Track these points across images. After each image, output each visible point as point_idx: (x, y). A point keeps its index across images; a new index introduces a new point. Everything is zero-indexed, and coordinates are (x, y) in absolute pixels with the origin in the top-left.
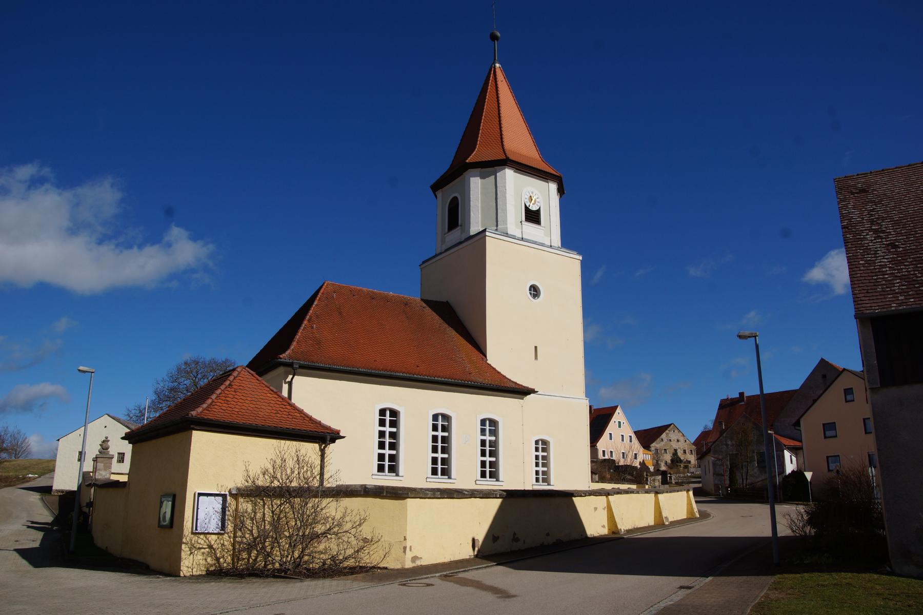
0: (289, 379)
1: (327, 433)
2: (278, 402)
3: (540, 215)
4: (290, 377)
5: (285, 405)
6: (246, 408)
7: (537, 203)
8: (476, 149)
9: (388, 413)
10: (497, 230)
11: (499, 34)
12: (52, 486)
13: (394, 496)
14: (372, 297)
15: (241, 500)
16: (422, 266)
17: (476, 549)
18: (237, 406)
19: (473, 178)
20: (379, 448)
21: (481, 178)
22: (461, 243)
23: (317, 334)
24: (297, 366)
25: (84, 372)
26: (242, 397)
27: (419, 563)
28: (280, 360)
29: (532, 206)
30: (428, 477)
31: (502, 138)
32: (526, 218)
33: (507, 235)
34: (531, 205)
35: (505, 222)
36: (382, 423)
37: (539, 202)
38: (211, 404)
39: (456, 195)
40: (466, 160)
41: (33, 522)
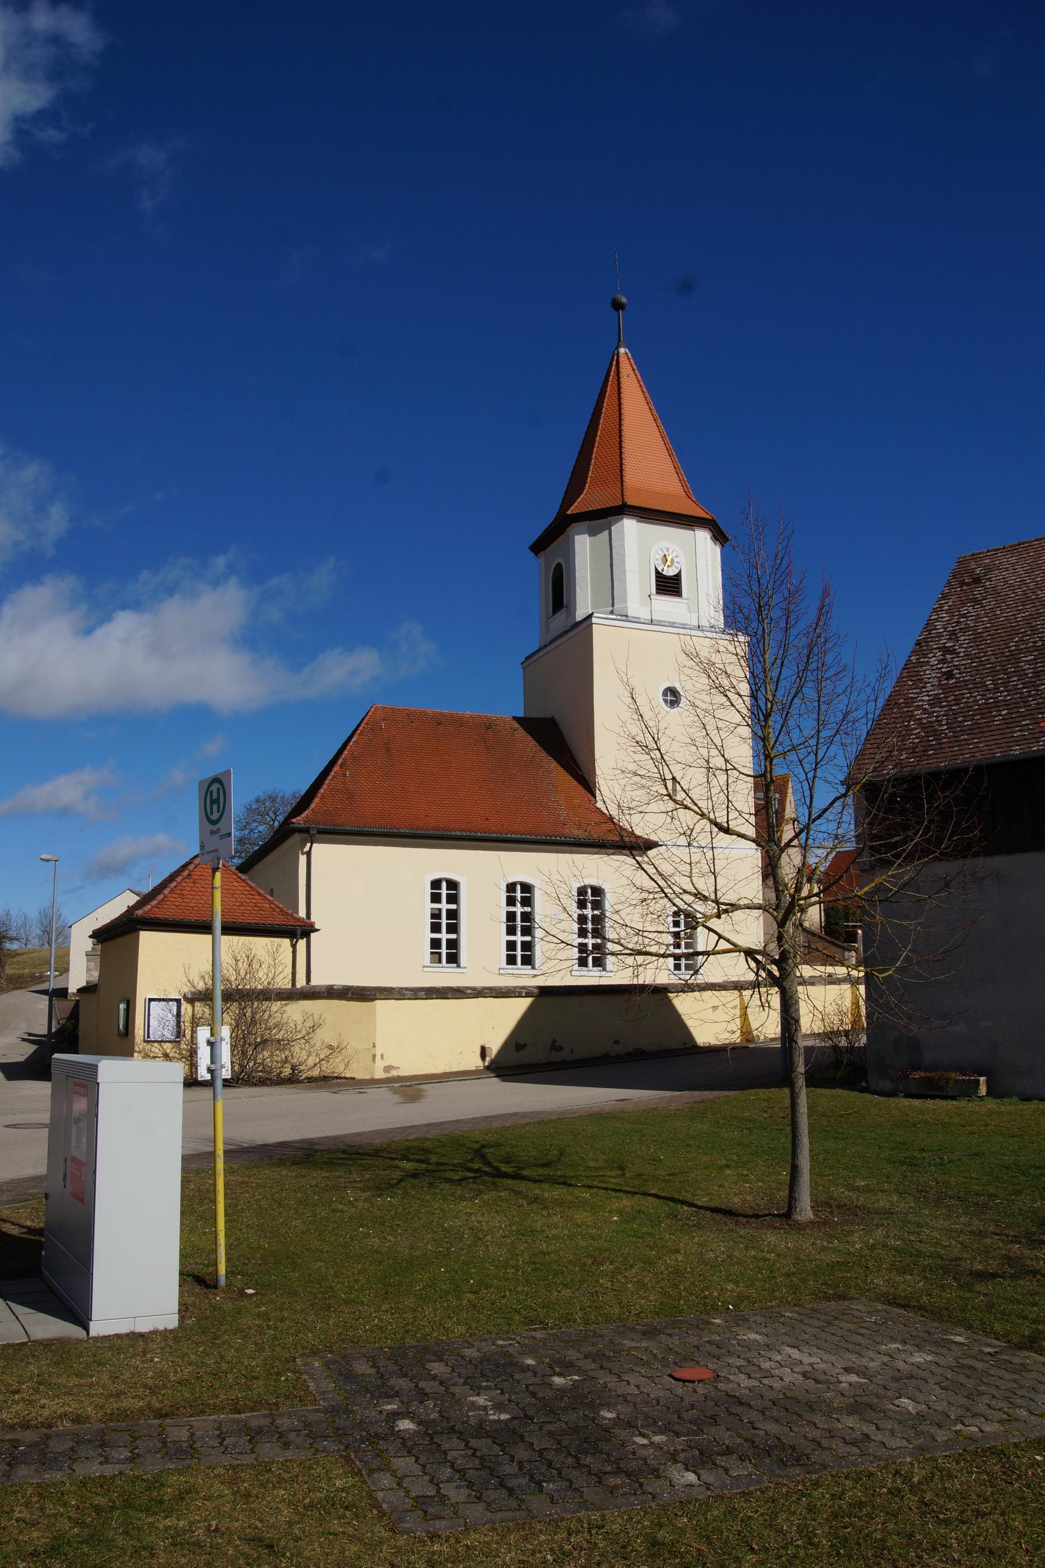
0: (307, 849)
2: (244, 892)
4: (309, 845)
6: (203, 902)
7: (675, 564)
8: (586, 491)
9: (444, 885)
10: (612, 613)
11: (624, 300)
12: (67, 989)
14: (440, 721)
15: (197, 1004)
17: (488, 1059)
18: (193, 901)
20: (508, 934)
22: (566, 632)
25: (48, 861)
26: (202, 889)
27: (394, 1073)
28: (292, 825)
29: (668, 571)
31: (621, 471)
32: (657, 589)
33: (625, 617)
34: (665, 568)
35: (624, 599)
36: (436, 898)
37: (678, 563)
38: (162, 900)
39: (560, 560)
40: (568, 510)
41: (30, 1035)
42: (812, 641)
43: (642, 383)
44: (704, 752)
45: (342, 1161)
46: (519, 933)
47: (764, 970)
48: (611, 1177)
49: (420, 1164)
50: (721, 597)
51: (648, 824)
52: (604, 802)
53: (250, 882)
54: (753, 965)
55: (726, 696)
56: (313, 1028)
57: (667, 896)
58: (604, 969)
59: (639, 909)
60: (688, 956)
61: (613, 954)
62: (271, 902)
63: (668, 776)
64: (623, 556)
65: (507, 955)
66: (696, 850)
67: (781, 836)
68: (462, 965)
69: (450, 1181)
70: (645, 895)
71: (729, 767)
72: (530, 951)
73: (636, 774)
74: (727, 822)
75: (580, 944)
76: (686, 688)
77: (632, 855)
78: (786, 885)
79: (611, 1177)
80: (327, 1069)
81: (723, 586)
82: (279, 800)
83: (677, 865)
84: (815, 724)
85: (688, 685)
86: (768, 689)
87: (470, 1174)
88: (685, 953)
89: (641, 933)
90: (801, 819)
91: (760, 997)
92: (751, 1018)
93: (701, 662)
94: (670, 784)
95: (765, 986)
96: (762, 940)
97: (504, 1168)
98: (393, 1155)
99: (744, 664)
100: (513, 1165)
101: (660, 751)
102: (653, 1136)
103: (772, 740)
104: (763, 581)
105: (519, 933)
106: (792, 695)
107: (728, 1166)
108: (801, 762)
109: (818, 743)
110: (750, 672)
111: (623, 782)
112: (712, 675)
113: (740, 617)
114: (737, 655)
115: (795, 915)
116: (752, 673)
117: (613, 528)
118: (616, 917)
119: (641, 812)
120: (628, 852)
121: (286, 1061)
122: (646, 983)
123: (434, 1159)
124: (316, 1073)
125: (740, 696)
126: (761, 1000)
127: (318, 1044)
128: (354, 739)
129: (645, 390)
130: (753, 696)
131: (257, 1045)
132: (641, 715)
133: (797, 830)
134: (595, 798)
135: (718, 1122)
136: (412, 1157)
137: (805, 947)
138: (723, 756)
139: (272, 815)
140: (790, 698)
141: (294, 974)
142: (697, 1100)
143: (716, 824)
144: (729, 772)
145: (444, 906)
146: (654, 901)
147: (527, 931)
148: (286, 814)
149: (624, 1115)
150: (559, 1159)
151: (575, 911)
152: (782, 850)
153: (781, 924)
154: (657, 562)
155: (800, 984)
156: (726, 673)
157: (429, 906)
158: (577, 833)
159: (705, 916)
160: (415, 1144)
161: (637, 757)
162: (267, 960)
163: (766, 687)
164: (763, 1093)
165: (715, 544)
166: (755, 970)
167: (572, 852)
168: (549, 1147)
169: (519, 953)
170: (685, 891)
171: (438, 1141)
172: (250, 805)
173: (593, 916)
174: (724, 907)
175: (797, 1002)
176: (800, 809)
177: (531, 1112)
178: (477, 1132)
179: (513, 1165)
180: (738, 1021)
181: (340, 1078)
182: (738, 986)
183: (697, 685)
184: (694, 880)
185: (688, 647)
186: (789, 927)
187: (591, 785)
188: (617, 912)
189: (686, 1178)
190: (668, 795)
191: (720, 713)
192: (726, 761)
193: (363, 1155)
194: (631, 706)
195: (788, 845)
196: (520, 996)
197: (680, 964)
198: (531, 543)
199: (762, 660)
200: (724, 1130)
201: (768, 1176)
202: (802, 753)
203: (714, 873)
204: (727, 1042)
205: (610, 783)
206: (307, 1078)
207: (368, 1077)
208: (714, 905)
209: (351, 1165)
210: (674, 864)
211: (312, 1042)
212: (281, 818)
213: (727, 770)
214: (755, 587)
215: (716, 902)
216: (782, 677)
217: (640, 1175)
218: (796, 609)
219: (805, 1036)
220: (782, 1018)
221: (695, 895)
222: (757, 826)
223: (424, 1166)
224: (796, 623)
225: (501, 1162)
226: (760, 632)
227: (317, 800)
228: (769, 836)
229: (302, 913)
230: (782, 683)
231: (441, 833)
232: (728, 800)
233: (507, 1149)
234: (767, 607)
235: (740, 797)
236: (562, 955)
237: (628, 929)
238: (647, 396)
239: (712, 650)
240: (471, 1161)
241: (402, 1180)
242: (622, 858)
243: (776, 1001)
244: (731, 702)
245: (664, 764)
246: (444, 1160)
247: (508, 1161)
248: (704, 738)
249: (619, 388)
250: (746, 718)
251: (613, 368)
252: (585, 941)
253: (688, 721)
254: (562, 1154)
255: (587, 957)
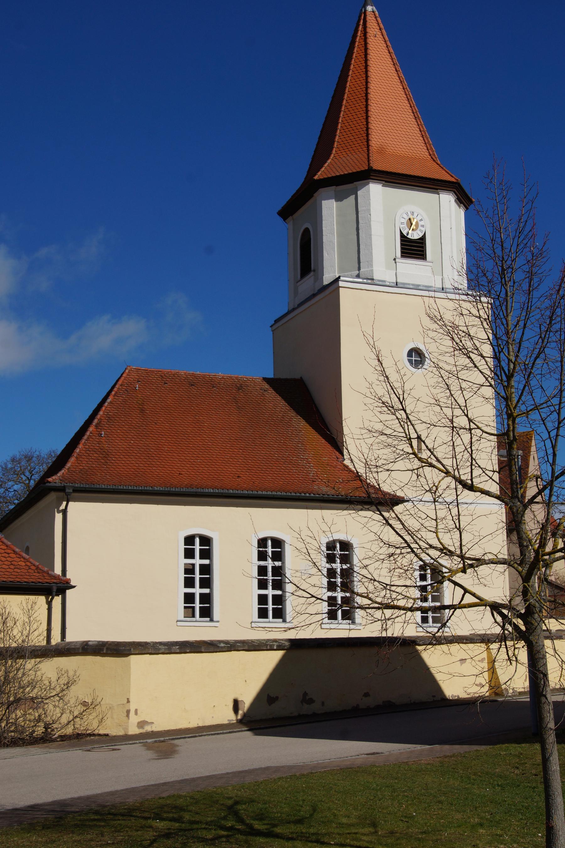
0: (63, 507)
1: (54, 583)
3: (425, 241)
4: (64, 503)
5: (8, 554)
7: (420, 228)
8: (332, 156)
9: (197, 540)
10: (358, 276)
13: (115, 653)
16: (274, 327)
17: (240, 712)
19: (326, 201)
21: (337, 200)
22: (314, 295)
23: (105, 443)
24: (71, 491)
27: (148, 728)
28: (48, 484)
30: (254, 620)
31: (368, 135)
32: (402, 252)
33: (371, 280)
34: (410, 232)
36: (189, 554)
37: (423, 226)
39: (307, 225)
40: (315, 175)
42: (555, 303)
43: (389, 43)
44: (448, 412)
45: (95, 823)
46: (270, 587)
47: (510, 624)
48: (364, 835)
49: (173, 823)
50: (465, 261)
51: (394, 481)
52: (352, 461)
53: (5, 541)
54: (499, 619)
55: (469, 357)
56: (68, 685)
57: (413, 551)
58: (354, 622)
59: (386, 564)
60: (435, 610)
61: (361, 607)
62: (26, 560)
63: (414, 435)
64: (369, 220)
65: (259, 608)
66: (441, 507)
67: (525, 492)
68: (215, 619)
69: (203, 840)
70: (392, 550)
71: (473, 426)
72: (281, 605)
73: (383, 434)
74: (472, 480)
75: (329, 598)
76: (430, 350)
77: (379, 510)
78: (530, 541)
79: (364, 835)
80: (81, 726)
81: (467, 250)
82: (34, 459)
83: (423, 521)
84: (557, 383)
85: (432, 347)
86: (511, 350)
87: (225, 833)
88: (432, 607)
89: (388, 587)
90: (545, 476)
91: (507, 651)
92: (499, 671)
93: (445, 325)
94: (415, 443)
95: (512, 640)
96: (508, 594)
97: (258, 825)
98: (146, 815)
99: (486, 326)
100: (266, 822)
101: (405, 411)
102: (404, 791)
103: (515, 400)
104: (507, 245)
105: (270, 587)
106: (534, 356)
107: (481, 825)
108: (543, 421)
109: (560, 403)
110: (493, 334)
111: (370, 441)
112: (455, 337)
113: (483, 281)
114: (480, 317)
115: (539, 569)
116: (495, 335)
117: (359, 193)
118: (364, 572)
119: (388, 470)
120: (374, 508)
121: (39, 720)
122: (395, 635)
123: (187, 817)
124: (69, 730)
125: (483, 357)
126: (508, 654)
127: (72, 701)
128: (109, 400)
129: (392, 50)
130: (496, 357)
131: (10, 704)
132: (387, 377)
133: (541, 487)
134: (343, 455)
135: (469, 778)
136: (165, 815)
137: (550, 601)
138: (467, 416)
139: (27, 474)
140: (533, 359)
141: (49, 630)
142: (448, 754)
143: (461, 482)
144: (473, 431)
145: (198, 561)
146: (401, 556)
147: (278, 585)
148: (42, 473)
149: (375, 769)
150: (311, 815)
151: (324, 565)
152: (525, 507)
153: (526, 579)
154: (402, 226)
155: (547, 638)
156: (469, 335)
157: (184, 561)
158: (325, 490)
159: (450, 570)
160: (168, 802)
161: (384, 417)
162: (21, 617)
163: (508, 348)
164: (514, 748)
165: (459, 207)
166: (502, 624)
167: (321, 508)
168: (301, 803)
169: (270, 606)
170: (431, 546)
171: (192, 798)
172: (6, 464)
173: (342, 570)
174: (470, 562)
175: (544, 657)
176: (544, 467)
177: (283, 767)
178: (230, 788)
179: (266, 822)
180: (486, 675)
181: (94, 735)
182: (485, 639)
183: (441, 347)
184: (440, 534)
185: (432, 310)
186: (535, 581)
187: (339, 444)
188: (366, 567)
189: (439, 837)
190: (414, 453)
191: (463, 375)
192: (470, 421)
193: (115, 815)
194: (377, 368)
195: (532, 501)
196: (272, 649)
197: (427, 617)
198: (279, 208)
199: (505, 322)
200: (476, 787)
201: (523, 838)
202: (545, 412)
203: (459, 529)
204: (477, 695)
205: (357, 442)
206: (60, 736)
207: (121, 733)
208: (460, 560)
209: (103, 826)
210: (420, 520)
211: (66, 699)
212: (37, 477)
213: (470, 430)
214: (499, 252)
215: (462, 557)
216: (525, 338)
217: (392, 833)
218: (539, 272)
219: (554, 690)
220: (530, 672)
221: (441, 550)
222: (501, 483)
223: (177, 825)
224: (539, 285)
225: (255, 819)
226: (503, 295)
227: (72, 459)
228: (513, 492)
229: (58, 570)
230: (524, 344)
231: (195, 490)
232: (472, 458)
233: (260, 806)
234: (510, 270)
235: (484, 455)
236: (312, 609)
237: (376, 583)
238: (394, 56)
239: (455, 313)
240: (225, 818)
241: (154, 841)
242: (369, 514)
243: (523, 655)
244: (474, 364)
245: (409, 423)
246: (197, 818)
247: (260, 817)
248: (448, 398)
249: (366, 49)
250: (489, 379)
251: (361, 28)
252: (334, 595)
253: (432, 382)
254: (314, 810)
255: (336, 611)
